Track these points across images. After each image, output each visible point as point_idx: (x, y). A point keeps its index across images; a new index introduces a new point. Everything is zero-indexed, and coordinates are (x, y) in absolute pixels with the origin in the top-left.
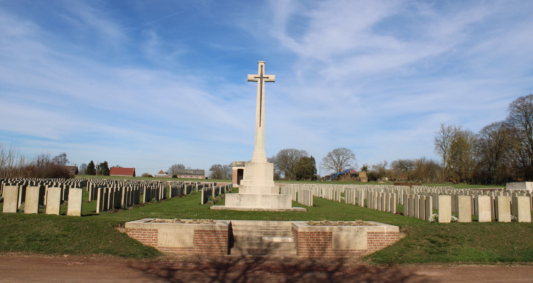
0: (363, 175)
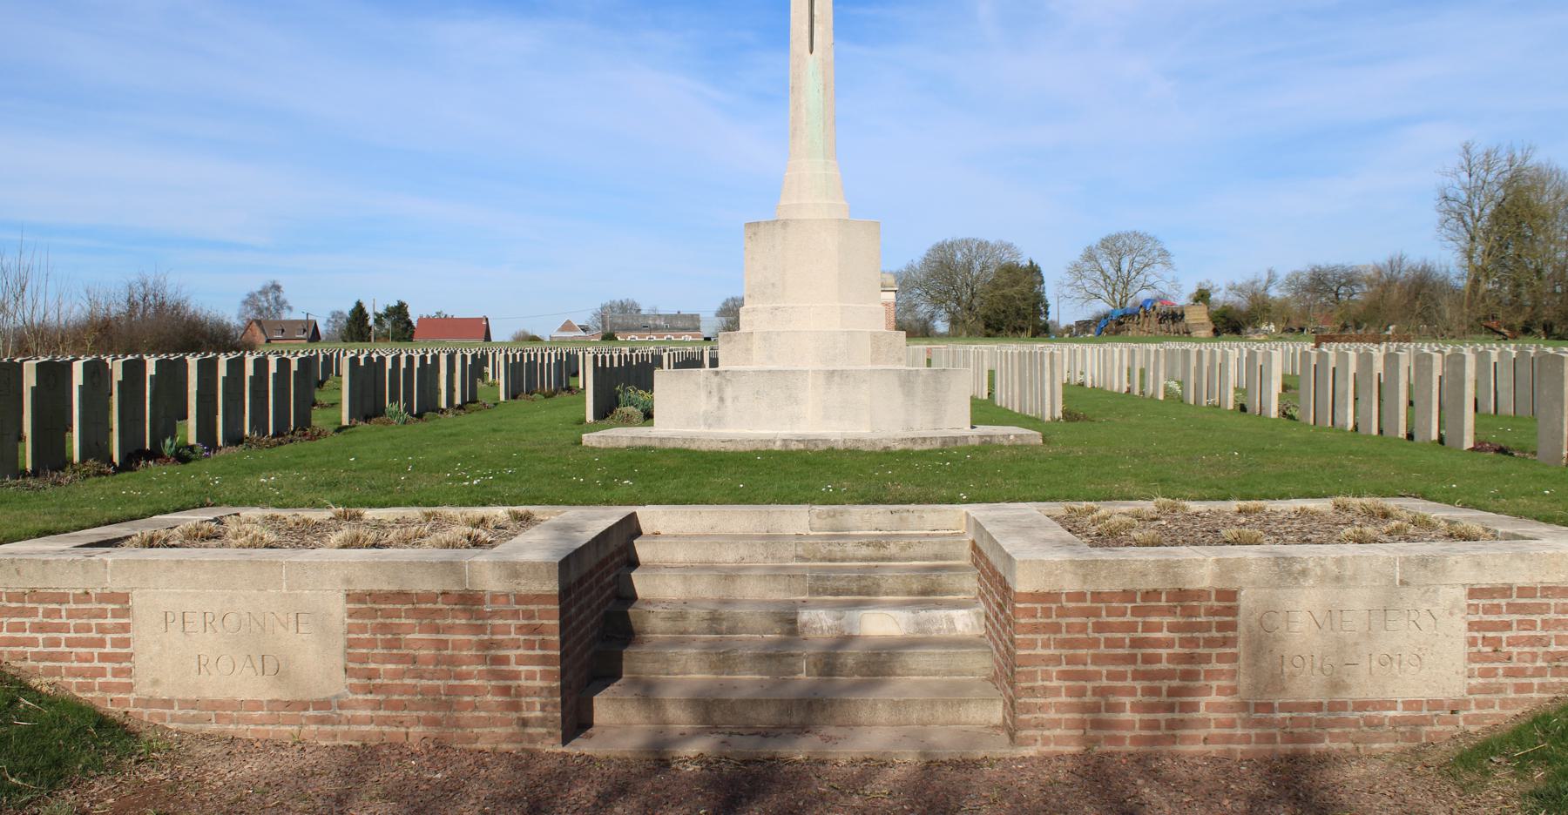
0: (1198, 316)
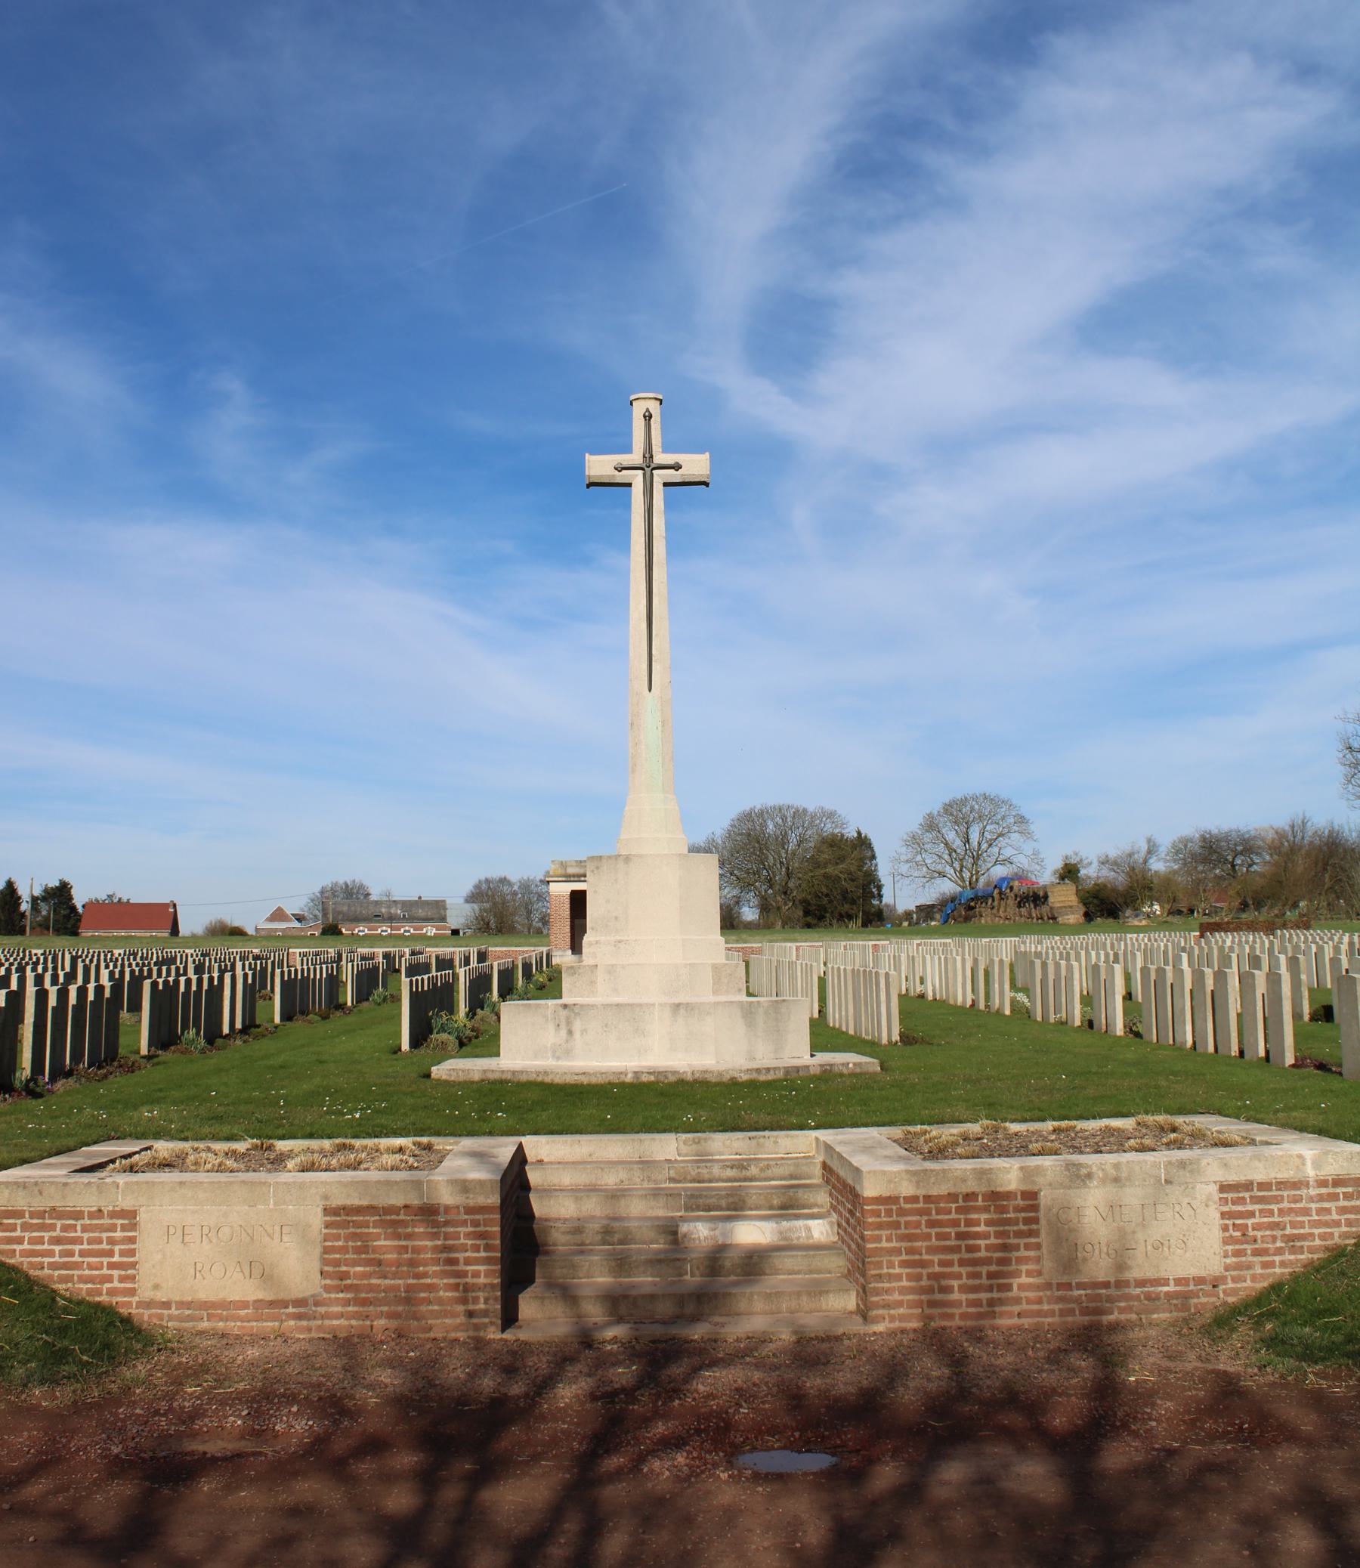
0: (1065, 897)
